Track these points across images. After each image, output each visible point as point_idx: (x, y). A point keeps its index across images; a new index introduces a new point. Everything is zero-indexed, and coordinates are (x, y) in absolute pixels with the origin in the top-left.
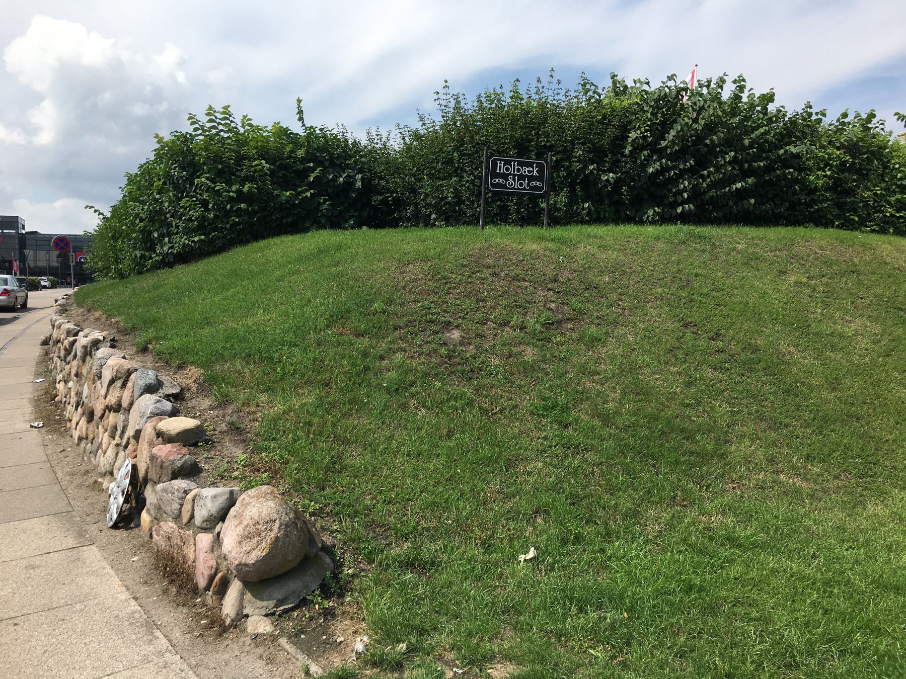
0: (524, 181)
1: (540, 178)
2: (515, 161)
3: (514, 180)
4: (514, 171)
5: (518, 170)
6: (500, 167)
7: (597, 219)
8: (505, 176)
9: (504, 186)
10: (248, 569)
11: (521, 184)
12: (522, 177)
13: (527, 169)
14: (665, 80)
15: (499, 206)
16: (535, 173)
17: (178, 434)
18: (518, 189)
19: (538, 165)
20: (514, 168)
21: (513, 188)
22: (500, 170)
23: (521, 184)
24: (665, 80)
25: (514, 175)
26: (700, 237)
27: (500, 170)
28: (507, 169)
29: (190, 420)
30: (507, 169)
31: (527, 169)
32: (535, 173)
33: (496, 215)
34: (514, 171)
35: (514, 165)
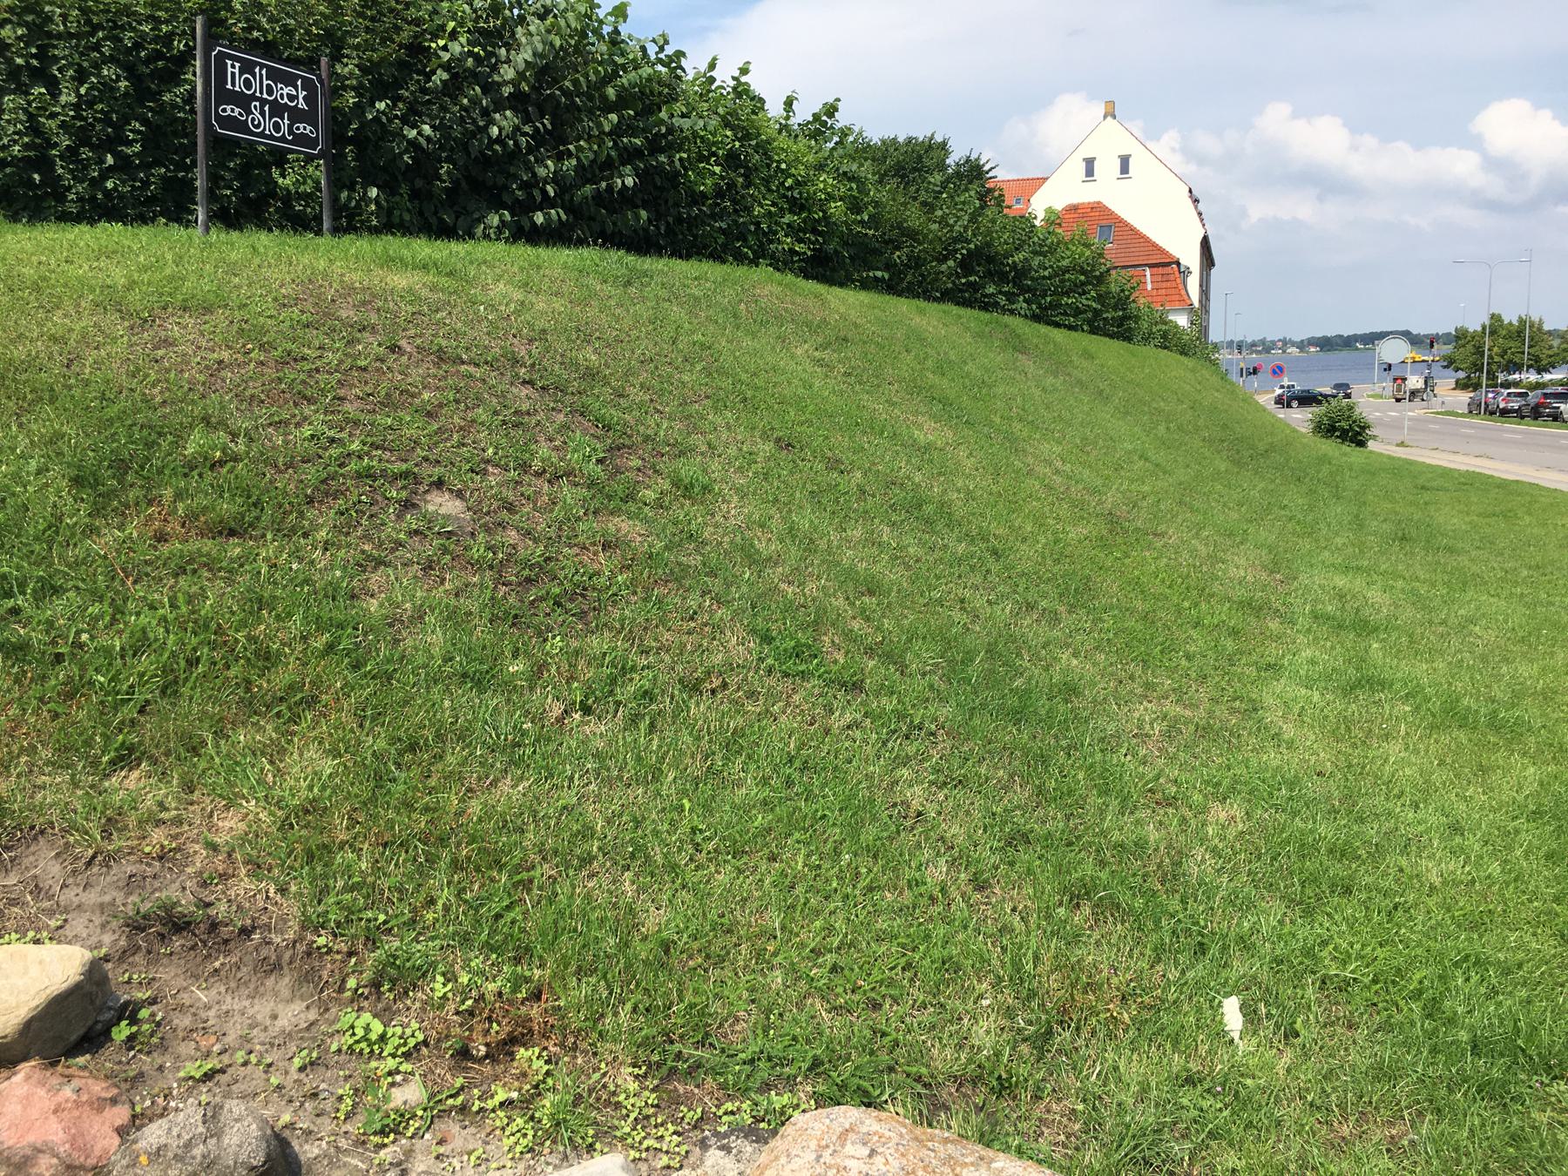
0: (282, 119)
1: (308, 117)
2: (262, 66)
3: (262, 113)
4: (261, 93)
5: (270, 92)
6: (233, 74)
7: (390, 225)
8: (243, 101)
9: (242, 127)
10: (1302, 208)
11: (277, 127)
12: (277, 109)
13: (286, 91)
14: (737, 74)
15: (163, 178)
16: (302, 105)
17: (28, 1025)
18: (271, 137)
19: (306, 85)
20: (260, 82)
21: (262, 135)
22: (233, 84)
23: (277, 127)
24: (737, 74)
25: (263, 102)
26: (425, 267)
27: (233, 84)
28: (248, 84)
29: (50, 950)
30: (248, 84)
31: (286, 91)
32: (302, 105)
33: (151, 201)
34: (261, 93)
35: (261, 75)
